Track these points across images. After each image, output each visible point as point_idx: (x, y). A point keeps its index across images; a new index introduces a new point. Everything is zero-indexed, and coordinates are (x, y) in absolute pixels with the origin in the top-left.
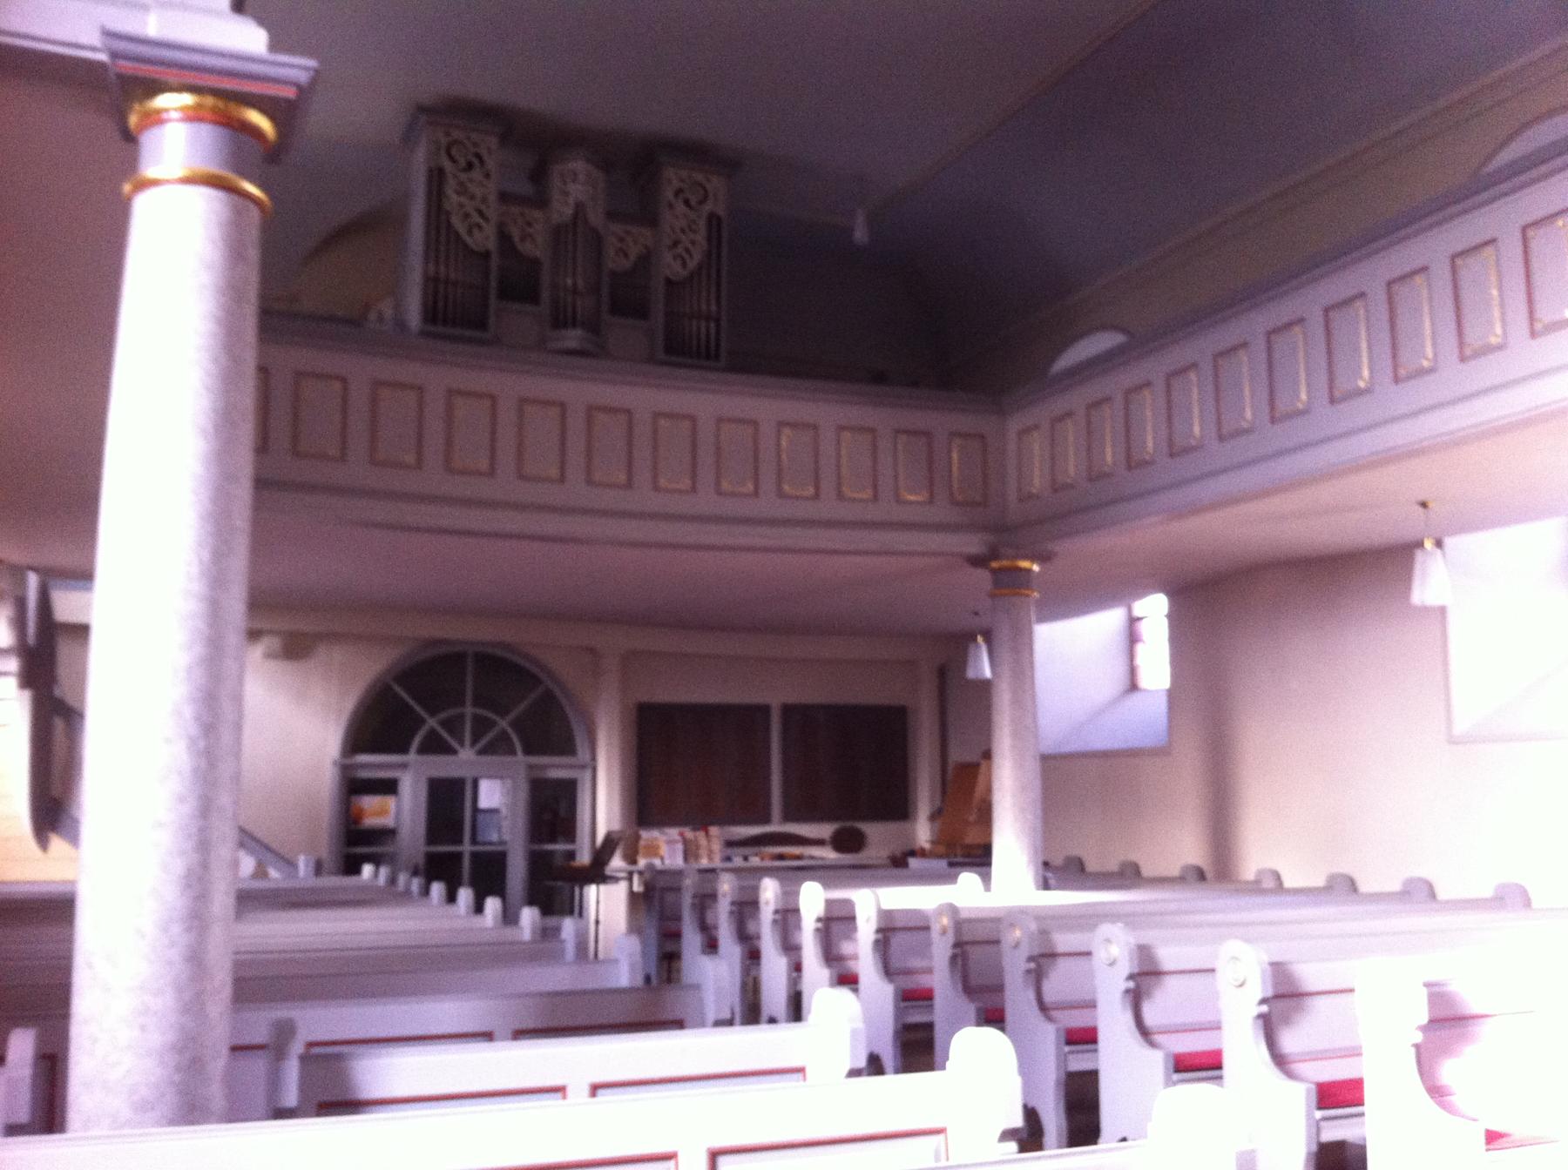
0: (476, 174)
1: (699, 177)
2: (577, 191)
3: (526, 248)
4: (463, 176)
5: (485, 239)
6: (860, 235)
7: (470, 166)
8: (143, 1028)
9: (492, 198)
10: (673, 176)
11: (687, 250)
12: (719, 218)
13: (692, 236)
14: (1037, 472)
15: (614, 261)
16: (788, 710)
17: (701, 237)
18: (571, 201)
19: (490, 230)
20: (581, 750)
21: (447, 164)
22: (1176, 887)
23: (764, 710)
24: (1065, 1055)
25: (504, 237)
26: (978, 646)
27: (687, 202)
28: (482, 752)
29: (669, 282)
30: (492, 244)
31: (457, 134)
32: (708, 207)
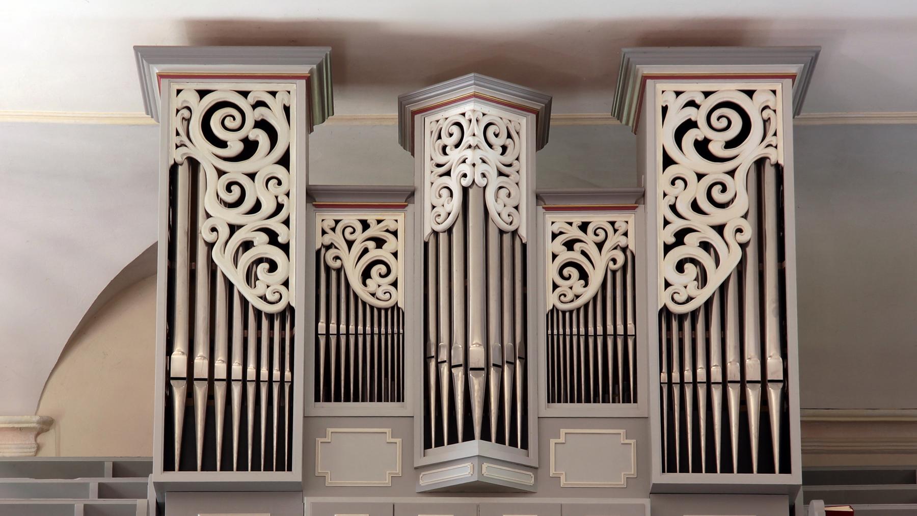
4: (236, 171)
7: (250, 148)
9: (295, 207)
11: (706, 246)
20: (361, 287)
22: (480, 392)
24: (318, 252)
27: (702, 147)
32: (750, 150)
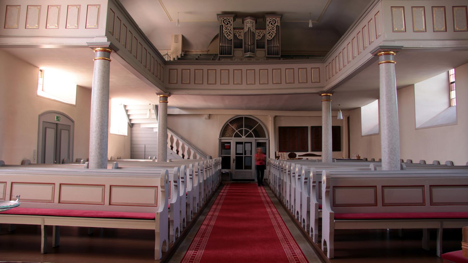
0: (229, 25)
1: (274, 18)
2: (249, 25)
3: (240, 38)
4: (226, 26)
5: (231, 37)
6: (310, 25)
7: (228, 24)
8: (94, 161)
9: (232, 29)
10: (268, 19)
11: (272, 33)
12: (279, 26)
13: (273, 31)
14: (331, 73)
15: (257, 38)
16: (312, 127)
17: (275, 31)
18: (247, 27)
19: (232, 35)
21: (223, 24)
23: (307, 127)
25: (235, 36)
26: (340, 112)
28: (246, 137)
29: (268, 40)
30: (232, 38)
31: (225, 18)
32: (276, 24)
